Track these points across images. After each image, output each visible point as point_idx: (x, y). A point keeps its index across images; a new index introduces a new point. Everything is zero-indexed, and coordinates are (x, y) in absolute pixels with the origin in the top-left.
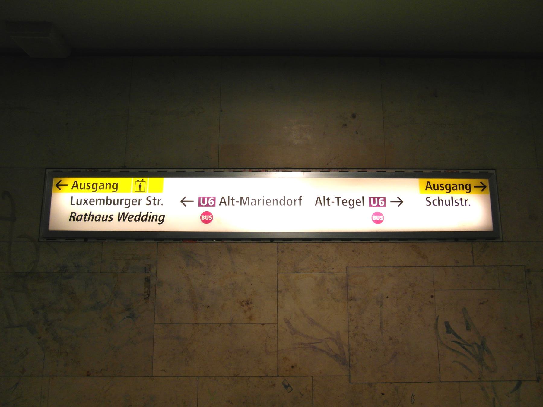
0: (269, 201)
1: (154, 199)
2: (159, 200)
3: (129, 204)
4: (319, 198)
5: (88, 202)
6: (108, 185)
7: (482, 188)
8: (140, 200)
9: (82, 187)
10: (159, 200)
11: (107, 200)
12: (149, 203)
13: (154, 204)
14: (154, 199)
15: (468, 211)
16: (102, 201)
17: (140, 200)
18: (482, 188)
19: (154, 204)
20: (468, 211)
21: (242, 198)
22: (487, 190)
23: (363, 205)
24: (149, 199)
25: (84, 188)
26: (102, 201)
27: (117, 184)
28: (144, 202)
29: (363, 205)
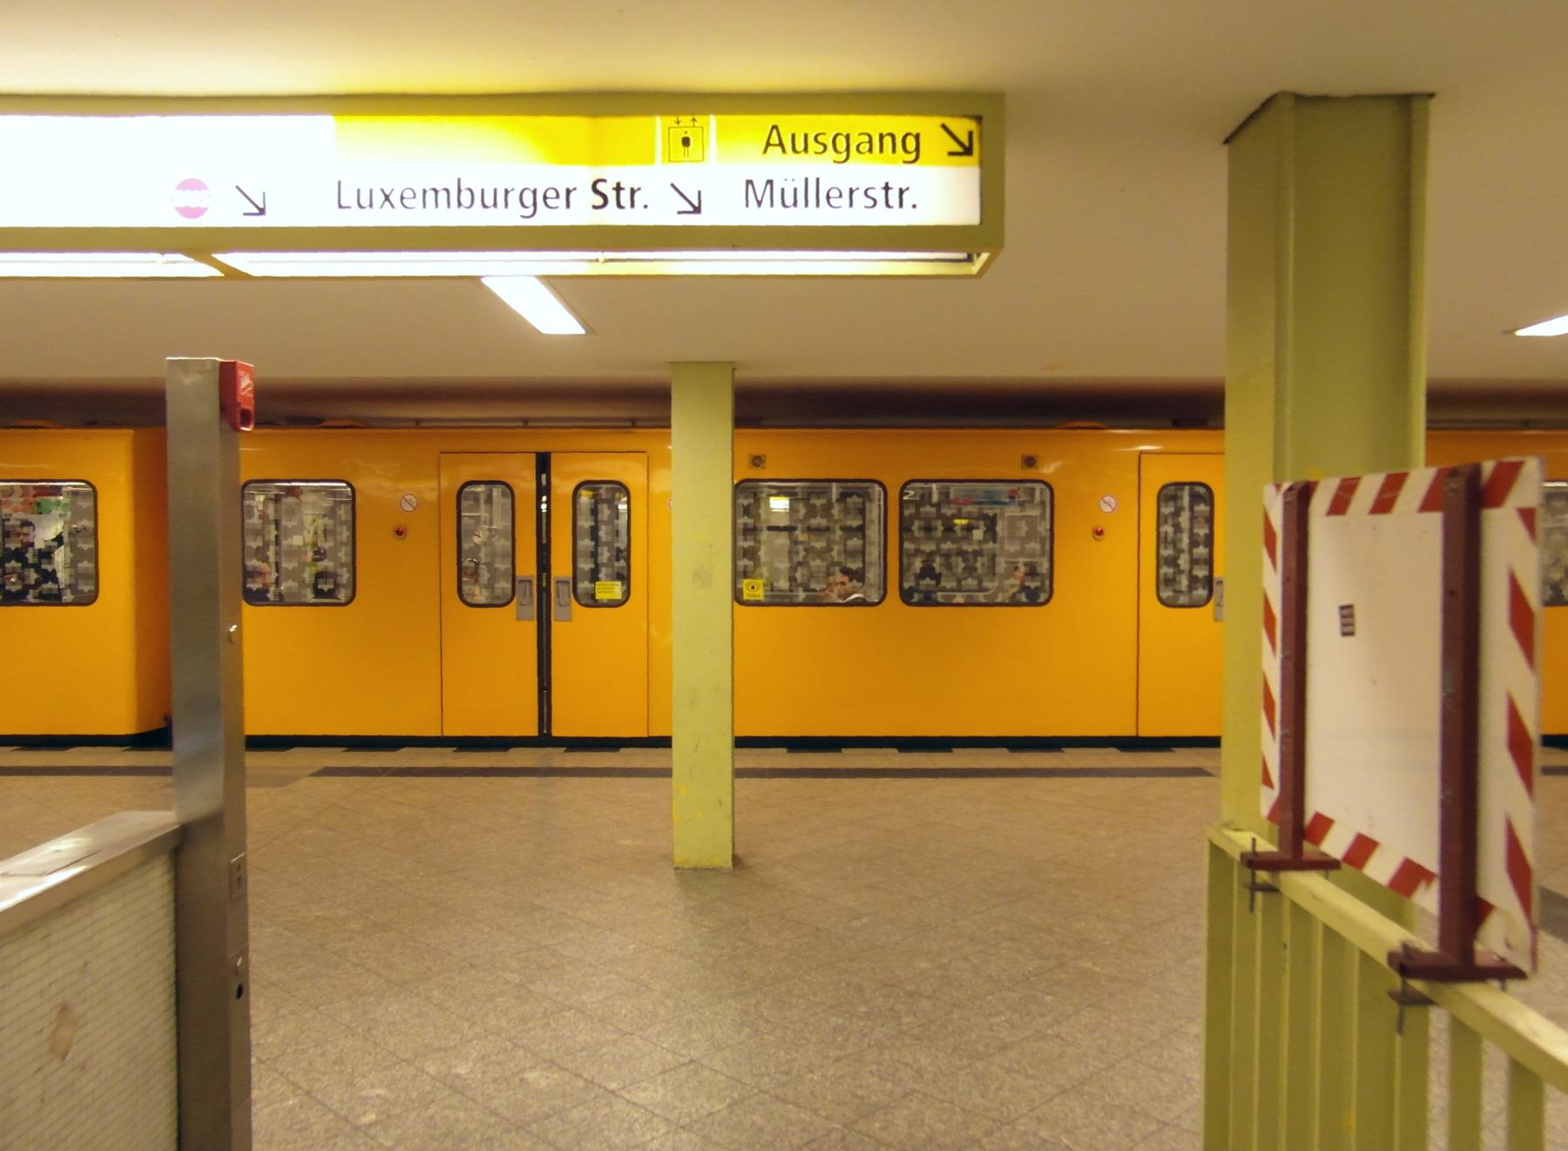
0: (551, 194)
1: (618, 188)
2: (633, 192)
3: (535, 204)
4: (749, 182)
5: (395, 198)
6: (888, 141)
7: (958, 149)
8: (568, 192)
9: (800, 145)
10: (633, 192)
11: (459, 191)
12: (600, 201)
13: (619, 205)
14: (618, 188)
15: (1520, 333)
16: (442, 196)
17: (568, 192)
18: (958, 149)
19: (619, 205)
20: (1520, 333)
21: (749, 182)
22: (975, 158)
23: (568, 206)
24: (600, 187)
25: (806, 149)
26: (442, 196)
27: (917, 137)
28: (585, 198)
29: (568, 206)
